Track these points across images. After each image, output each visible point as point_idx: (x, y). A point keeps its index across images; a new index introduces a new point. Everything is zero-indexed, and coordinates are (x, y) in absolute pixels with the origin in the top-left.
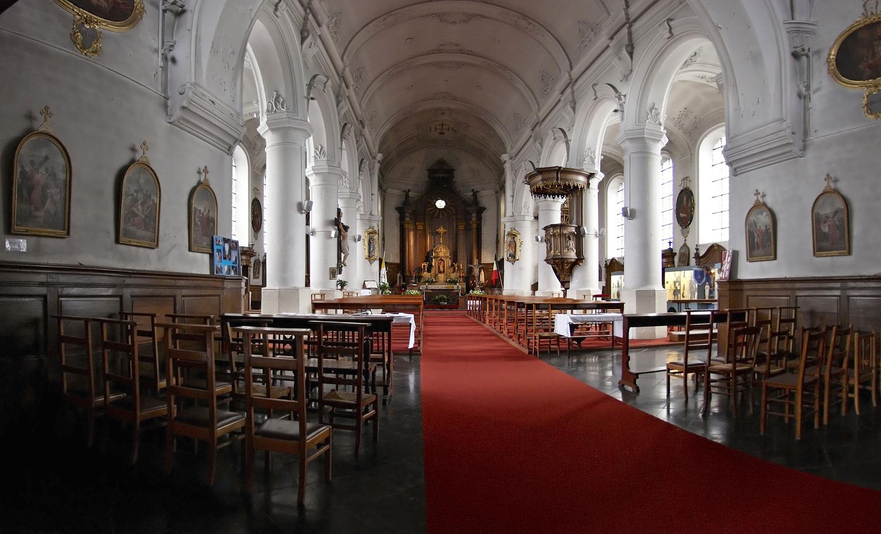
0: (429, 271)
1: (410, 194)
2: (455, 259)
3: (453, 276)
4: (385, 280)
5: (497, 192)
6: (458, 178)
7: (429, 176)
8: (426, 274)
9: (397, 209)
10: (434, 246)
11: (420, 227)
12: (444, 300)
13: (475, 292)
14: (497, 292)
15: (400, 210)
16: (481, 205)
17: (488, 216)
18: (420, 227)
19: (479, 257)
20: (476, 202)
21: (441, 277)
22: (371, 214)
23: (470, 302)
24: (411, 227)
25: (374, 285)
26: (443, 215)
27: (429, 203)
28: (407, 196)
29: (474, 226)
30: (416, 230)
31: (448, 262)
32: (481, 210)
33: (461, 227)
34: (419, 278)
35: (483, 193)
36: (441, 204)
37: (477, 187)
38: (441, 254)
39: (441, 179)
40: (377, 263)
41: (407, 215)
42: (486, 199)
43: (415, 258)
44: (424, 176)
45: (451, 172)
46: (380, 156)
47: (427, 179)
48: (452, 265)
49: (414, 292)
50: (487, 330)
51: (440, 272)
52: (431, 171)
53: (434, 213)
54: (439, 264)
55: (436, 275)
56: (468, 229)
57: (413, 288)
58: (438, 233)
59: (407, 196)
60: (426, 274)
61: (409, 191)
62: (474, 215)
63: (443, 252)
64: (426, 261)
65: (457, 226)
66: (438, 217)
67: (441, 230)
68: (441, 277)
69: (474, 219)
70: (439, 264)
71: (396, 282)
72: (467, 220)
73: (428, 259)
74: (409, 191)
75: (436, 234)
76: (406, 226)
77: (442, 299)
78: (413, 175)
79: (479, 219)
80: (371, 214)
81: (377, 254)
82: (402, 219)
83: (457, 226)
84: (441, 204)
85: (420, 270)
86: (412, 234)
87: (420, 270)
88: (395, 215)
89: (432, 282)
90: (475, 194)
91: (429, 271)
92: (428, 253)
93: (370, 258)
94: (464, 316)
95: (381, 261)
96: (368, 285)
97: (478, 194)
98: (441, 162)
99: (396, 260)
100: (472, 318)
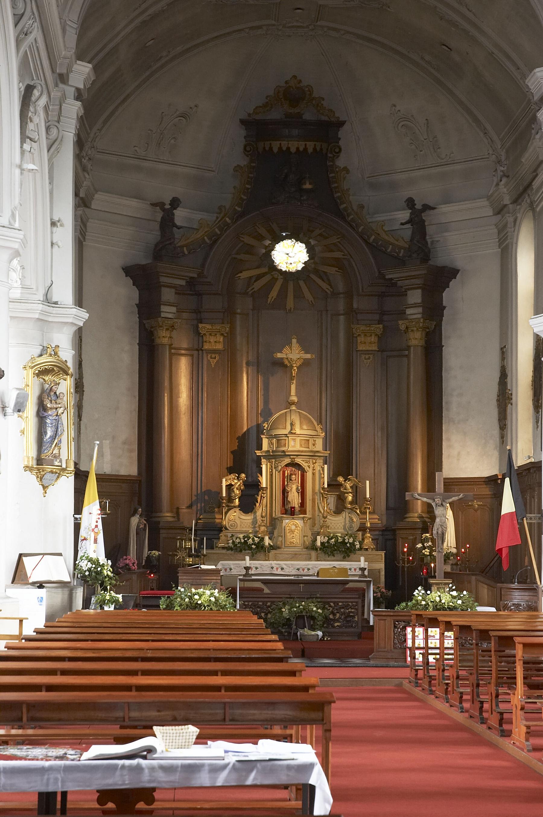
0: (248, 506)
1: (180, 216)
2: (343, 462)
3: (338, 525)
4: (95, 549)
5: (500, 211)
6: (354, 156)
7: (249, 149)
8: (236, 520)
9: (128, 271)
10: (267, 414)
11: (215, 342)
12: (311, 621)
13: (434, 595)
14: (518, 597)
15: (143, 277)
16: (441, 259)
17: (466, 301)
18: (215, 342)
19: (434, 461)
20: (420, 245)
21: (295, 529)
22: (48, 300)
23: (416, 636)
24: (183, 341)
25: (60, 570)
26: (299, 295)
27: (249, 250)
28: (167, 223)
29: (416, 339)
30: (197, 353)
31: (319, 474)
32: (442, 277)
33: (368, 343)
34: (211, 532)
35: (447, 212)
36: (290, 255)
37: (424, 191)
38: (294, 445)
39: (291, 161)
40: (67, 484)
41: (168, 294)
42: (459, 236)
43: (196, 455)
44: (228, 149)
45: (328, 131)
46: (82, 73)
47: (243, 162)
48: (334, 485)
49: (206, 595)
50: (525, 771)
51: (291, 512)
52: (257, 130)
53: (269, 286)
54: (286, 480)
55: (273, 524)
56: (390, 350)
57: (201, 579)
58: (281, 364)
59: (167, 223)
60: (236, 520)
61: (175, 203)
62: (415, 297)
63: (300, 435)
64: (235, 468)
65: (351, 339)
66: (280, 303)
67: (294, 354)
68: (295, 529)
69: (414, 313)
70: (286, 480)
71: (126, 552)
72: (388, 319)
73: (243, 458)
74: (175, 203)
75: (271, 367)
76: (163, 337)
77: (305, 619)
78: (198, 152)
79: (434, 311)
80: (48, 300)
81: (65, 452)
82: (147, 311)
83: (351, 339)
84: (290, 255)
85: (213, 502)
86: (183, 366)
87: (213, 502)
88: (125, 293)
89: (258, 550)
90: (418, 214)
91: (248, 506)
92: (243, 439)
93: (42, 464)
94: (400, 693)
95: (81, 478)
96: (36, 570)
97: (427, 216)
98: (294, 94)
99: (128, 466)
100: (441, 706)
